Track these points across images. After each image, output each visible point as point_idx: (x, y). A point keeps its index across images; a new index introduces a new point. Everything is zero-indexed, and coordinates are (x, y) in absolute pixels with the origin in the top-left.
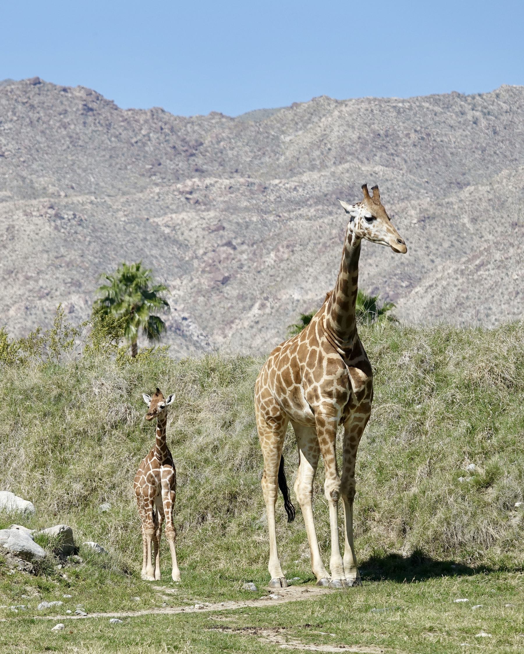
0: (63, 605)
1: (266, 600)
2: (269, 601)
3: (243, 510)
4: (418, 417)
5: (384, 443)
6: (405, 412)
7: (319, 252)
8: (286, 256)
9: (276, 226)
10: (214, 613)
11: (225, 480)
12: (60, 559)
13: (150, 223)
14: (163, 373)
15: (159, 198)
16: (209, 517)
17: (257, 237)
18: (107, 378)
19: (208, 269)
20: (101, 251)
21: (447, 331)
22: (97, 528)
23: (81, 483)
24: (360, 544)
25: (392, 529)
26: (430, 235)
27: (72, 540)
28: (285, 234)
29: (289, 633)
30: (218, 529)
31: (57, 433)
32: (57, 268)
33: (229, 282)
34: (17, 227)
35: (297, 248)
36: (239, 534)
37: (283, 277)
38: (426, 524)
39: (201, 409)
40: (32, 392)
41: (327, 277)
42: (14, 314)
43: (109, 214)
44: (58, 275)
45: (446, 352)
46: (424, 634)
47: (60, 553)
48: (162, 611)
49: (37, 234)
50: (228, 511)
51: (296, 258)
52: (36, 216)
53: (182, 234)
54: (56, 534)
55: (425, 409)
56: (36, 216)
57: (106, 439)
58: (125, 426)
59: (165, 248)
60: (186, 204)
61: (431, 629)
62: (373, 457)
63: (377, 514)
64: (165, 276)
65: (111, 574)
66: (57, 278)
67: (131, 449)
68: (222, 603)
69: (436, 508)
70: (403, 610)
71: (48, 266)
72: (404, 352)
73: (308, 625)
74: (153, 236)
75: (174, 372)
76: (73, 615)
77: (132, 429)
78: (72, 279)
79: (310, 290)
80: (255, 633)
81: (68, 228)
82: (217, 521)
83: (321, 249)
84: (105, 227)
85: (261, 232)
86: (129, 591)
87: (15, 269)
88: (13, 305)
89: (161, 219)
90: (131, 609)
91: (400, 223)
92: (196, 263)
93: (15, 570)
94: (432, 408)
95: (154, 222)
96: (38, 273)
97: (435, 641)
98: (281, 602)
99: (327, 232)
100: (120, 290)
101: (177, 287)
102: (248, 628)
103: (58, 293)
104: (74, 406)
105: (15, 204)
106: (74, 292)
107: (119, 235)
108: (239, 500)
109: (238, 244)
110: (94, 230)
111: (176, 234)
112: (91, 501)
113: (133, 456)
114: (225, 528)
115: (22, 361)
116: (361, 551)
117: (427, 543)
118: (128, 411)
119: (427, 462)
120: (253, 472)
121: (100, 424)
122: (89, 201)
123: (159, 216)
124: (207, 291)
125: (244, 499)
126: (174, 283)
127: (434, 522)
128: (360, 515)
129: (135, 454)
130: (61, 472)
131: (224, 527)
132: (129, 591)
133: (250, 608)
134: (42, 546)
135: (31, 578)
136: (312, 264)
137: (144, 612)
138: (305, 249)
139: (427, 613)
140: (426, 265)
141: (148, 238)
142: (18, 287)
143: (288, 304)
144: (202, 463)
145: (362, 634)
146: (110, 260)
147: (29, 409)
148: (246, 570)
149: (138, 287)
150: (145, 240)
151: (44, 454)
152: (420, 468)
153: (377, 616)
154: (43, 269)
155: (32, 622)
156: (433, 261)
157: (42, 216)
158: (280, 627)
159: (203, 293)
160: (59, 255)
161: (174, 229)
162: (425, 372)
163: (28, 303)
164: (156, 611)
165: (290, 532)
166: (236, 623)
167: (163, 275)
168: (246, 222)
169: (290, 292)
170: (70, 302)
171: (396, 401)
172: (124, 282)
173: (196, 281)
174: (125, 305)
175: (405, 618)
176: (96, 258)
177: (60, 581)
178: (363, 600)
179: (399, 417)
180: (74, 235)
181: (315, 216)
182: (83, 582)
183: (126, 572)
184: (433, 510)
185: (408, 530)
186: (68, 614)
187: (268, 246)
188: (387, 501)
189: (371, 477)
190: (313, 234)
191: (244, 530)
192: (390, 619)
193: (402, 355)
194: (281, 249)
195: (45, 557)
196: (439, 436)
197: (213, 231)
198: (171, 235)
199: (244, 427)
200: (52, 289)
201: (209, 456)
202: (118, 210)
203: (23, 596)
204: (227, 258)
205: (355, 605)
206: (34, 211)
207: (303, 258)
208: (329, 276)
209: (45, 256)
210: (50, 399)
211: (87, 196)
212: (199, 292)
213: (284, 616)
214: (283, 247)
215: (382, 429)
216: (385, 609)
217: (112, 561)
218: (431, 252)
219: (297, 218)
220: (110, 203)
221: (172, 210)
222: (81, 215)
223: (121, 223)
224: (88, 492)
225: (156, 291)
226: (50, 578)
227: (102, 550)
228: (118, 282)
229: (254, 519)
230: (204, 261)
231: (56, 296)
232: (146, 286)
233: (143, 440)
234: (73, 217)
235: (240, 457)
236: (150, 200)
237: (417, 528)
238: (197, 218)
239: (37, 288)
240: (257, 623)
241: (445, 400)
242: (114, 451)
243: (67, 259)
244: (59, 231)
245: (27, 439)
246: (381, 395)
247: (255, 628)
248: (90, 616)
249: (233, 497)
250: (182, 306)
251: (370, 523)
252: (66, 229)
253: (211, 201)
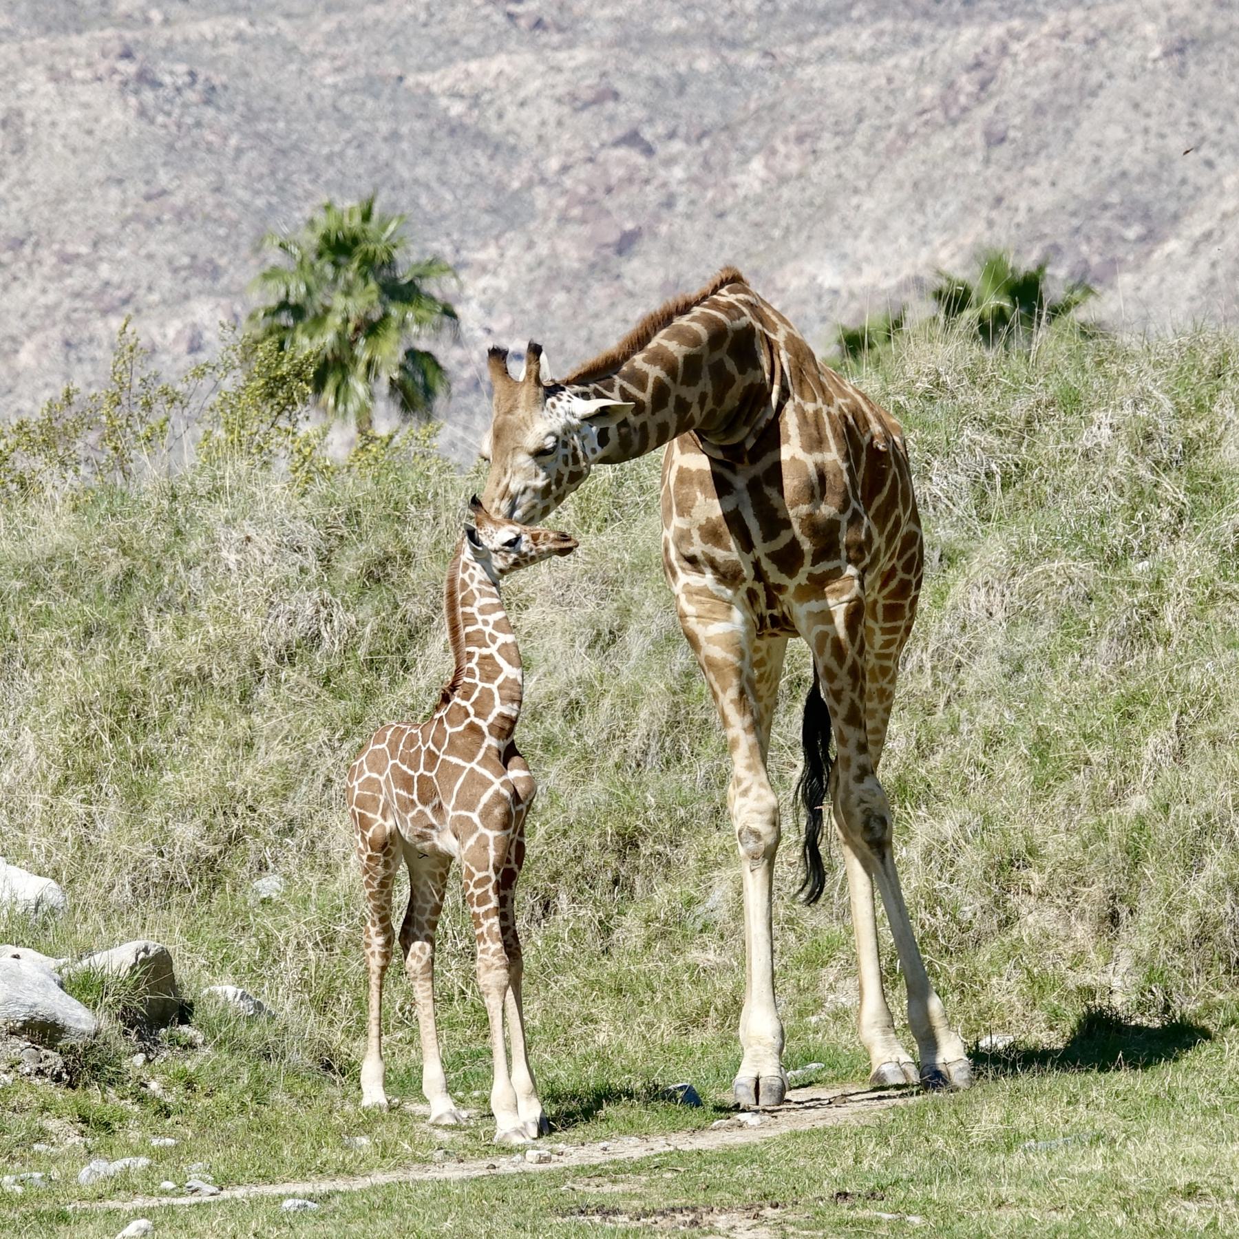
0: (150, 1167)
1: (729, 1128)
2: (737, 1132)
3: (657, 878)
4: (1141, 595)
5: (1048, 672)
6: (1105, 582)
7: (889, 151)
8: (793, 166)
9: (764, 84)
10: (580, 1171)
11: (604, 797)
12: (141, 1038)
13: (407, 90)
14: (419, 500)
15: (432, 15)
16: (563, 901)
17: (712, 116)
18: (259, 523)
19: (576, 212)
20: (273, 173)
21: (1216, 350)
22: (247, 947)
23: (197, 821)
24: (990, 962)
25: (1081, 917)
26: (1199, 90)
27: (171, 984)
28: (790, 104)
29: (791, 1218)
30: (589, 936)
31: (125, 682)
32: (149, 226)
33: (636, 248)
34: (29, 116)
35: (827, 143)
36: (648, 946)
37: (787, 230)
38: (1176, 897)
39: (529, 599)
40: (49, 569)
41: (912, 223)
42: (33, 363)
43: (293, 67)
44: (152, 247)
45: (1216, 408)
46: (1172, 1204)
47: (138, 1022)
48: (434, 1173)
49: (90, 132)
50: (616, 882)
51: (823, 171)
52: (84, 82)
53: (500, 116)
54: (125, 968)
55: (1160, 571)
56: (84, 82)
57: (263, 693)
58: (317, 657)
59: (451, 157)
60: (506, 31)
61: (1191, 1192)
62: (1020, 715)
63: (1034, 875)
64: (456, 236)
65: (287, 1075)
66: (150, 257)
67: (337, 720)
68: (605, 1144)
69: (1203, 851)
70: (1114, 1140)
71: (125, 223)
72: (1095, 415)
73: (844, 1195)
74: (418, 125)
75: (451, 496)
76: (180, 1195)
77: (337, 664)
78: (194, 257)
79: (867, 259)
80: (694, 1223)
81: (177, 112)
82: (586, 912)
83: (893, 142)
84: (280, 107)
85: (725, 100)
86: (337, 1120)
87: (30, 234)
88: (28, 336)
89: (437, 75)
90: (344, 1170)
91: (1114, 59)
92: (540, 196)
93: (12, 1075)
94: (1181, 567)
95: (418, 85)
96: (95, 245)
97: (1202, 1223)
98: (770, 1133)
99: (909, 94)
100: (321, 278)
101: (491, 267)
102: (673, 1210)
103: (155, 297)
104: (168, 603)
105: (22, 51)
106: (200, 292)
107: (322, 127)
108: (645, 850)
109: (658, 138)
110: (251, 116)
111: (482, 114)
112: (228, 873)
113: (341, 740)
114: (609, 931)
115: (23, 485)
116: (994, 980)
117: (1181, 950)
118: (324, 613)
119: (1174, 719)
120: (682, 771)
121: (245, 652)
122: (231, 33)
123: (433, 69)
124: (576, 276)
125: (660, 848)
126: (481, 256)
127: (1197, 889)
128: (989, 880)
129: (347, 733)
130: (140, 794)
131: (605, 929)
132: (337, 1120)
133: (680, 1154)
134: (86, 1003)
135: (59, 1094)
136: (869, 185)
137: (380, 1178)
138: (848, 144)
139: (1180, 1147)
140: (1191, 174)
141: (404, 130)
142: (38, 283)
143: (804, 302)
144: (538, 752)
145: (996, 1213)
146: (296, 198)
147: (42, 618)
148: (670, 1049)
149: (370, 265)
150: (394, 137)
151: (90, 743)
152: (1152, 740)
153: (1040, 1163)
154: (110, 231)
155: (63, 1217)
156: (1209, 164)
157: (100, 79)
158: (766, 1203)
159: (567, 281)
160: (154, 191)
161: (475, 101)
162: (1160, 466)
163: (69, 330)
164: (416, 1174)
165: (792, 937)
166: (640, 1197)
167: (448, 235)
168: (679, 76)
169: (810, 268)
170: (190, 319)
171: (1077, 552)
172: (328, 257)
173: (543, 249)
174: (335, 321)
175: (1118, 1164)
176: (257, 193)
177: (141, 1100)
178: (997, 1118)
179: (1089, 598)
180: (195, 132)
181: (873, 50)
182: (208, 1101)
183: (329, 1067)
184: (1193, 858)
185: (1123, 915)
186: (165, 1193)
187: (743, 141)
188: (1062, 837)
189: (1015, 770)
190: (869, 102)
191: (663, 935)
192: (1075, 1169)
193: (1092, 421)
194: (782, 149)
195: (96, 1034)
196: (1203, 645)
197: (586, 105)
198: (468, 121)
199: (653, 643)
200: (138, 287)
201: (556, 729)
202: (315, 56)
203: (36, 1147)
204: (630, 180)
205: (977, 1133)
206: (77, 66)
207: (843, 169)
208: (920, 220)
209: (114, 193)
210: (100, 586)
211: (226, 20)
212: (554, 278)
213: (776, 1172)
214: (786, 140)
215: (1042, 632)
216: (1061, 1141)
217: (288, 1039)
218: (1203, 139)
219: (822, 58)
220: (291, 37)
221: (469, 49)
222: (212, 74)
223: (325, 92)
224: (219, 848)
225: (420, 276)
226: (112, 1092)
227: (259, 1006)
228: (313, 256)
229: (690, 902)
230: (565, 192)
231: (149, 307)
232: (391, 264)
233: (370, 694)
234: (187, 79)
235: (642, 729)
236: (405, 23)
237: (1150, 909)
238: (541, 68)
239: (96, 285)
240: (701, 1196)
241: (1216, 545)
242: (287, 727)
243: (178, 200)
244: (152, 122)
245: (40, 704)
246: (1035, 538)
247: (694, 1210)
248: (226, 1194)
249: (628, 842)
250: (507, 320)
251: (1016, 900)
252: (169, 114)
253: (576, 21)
